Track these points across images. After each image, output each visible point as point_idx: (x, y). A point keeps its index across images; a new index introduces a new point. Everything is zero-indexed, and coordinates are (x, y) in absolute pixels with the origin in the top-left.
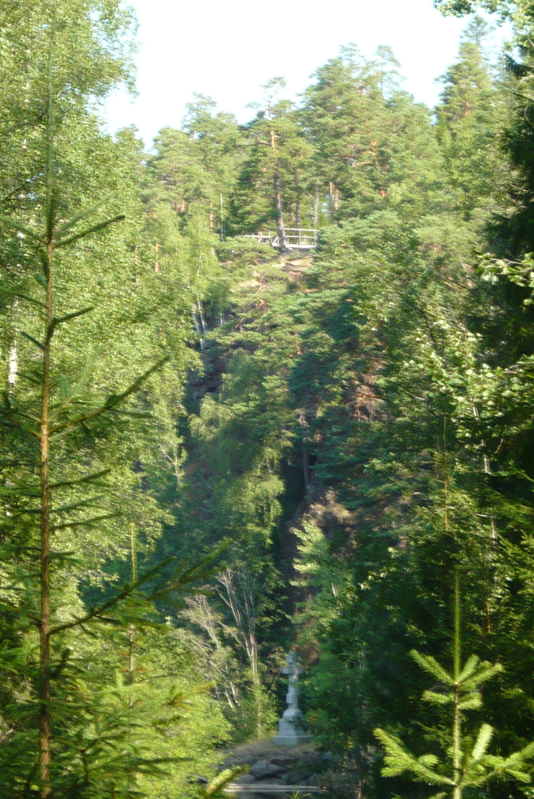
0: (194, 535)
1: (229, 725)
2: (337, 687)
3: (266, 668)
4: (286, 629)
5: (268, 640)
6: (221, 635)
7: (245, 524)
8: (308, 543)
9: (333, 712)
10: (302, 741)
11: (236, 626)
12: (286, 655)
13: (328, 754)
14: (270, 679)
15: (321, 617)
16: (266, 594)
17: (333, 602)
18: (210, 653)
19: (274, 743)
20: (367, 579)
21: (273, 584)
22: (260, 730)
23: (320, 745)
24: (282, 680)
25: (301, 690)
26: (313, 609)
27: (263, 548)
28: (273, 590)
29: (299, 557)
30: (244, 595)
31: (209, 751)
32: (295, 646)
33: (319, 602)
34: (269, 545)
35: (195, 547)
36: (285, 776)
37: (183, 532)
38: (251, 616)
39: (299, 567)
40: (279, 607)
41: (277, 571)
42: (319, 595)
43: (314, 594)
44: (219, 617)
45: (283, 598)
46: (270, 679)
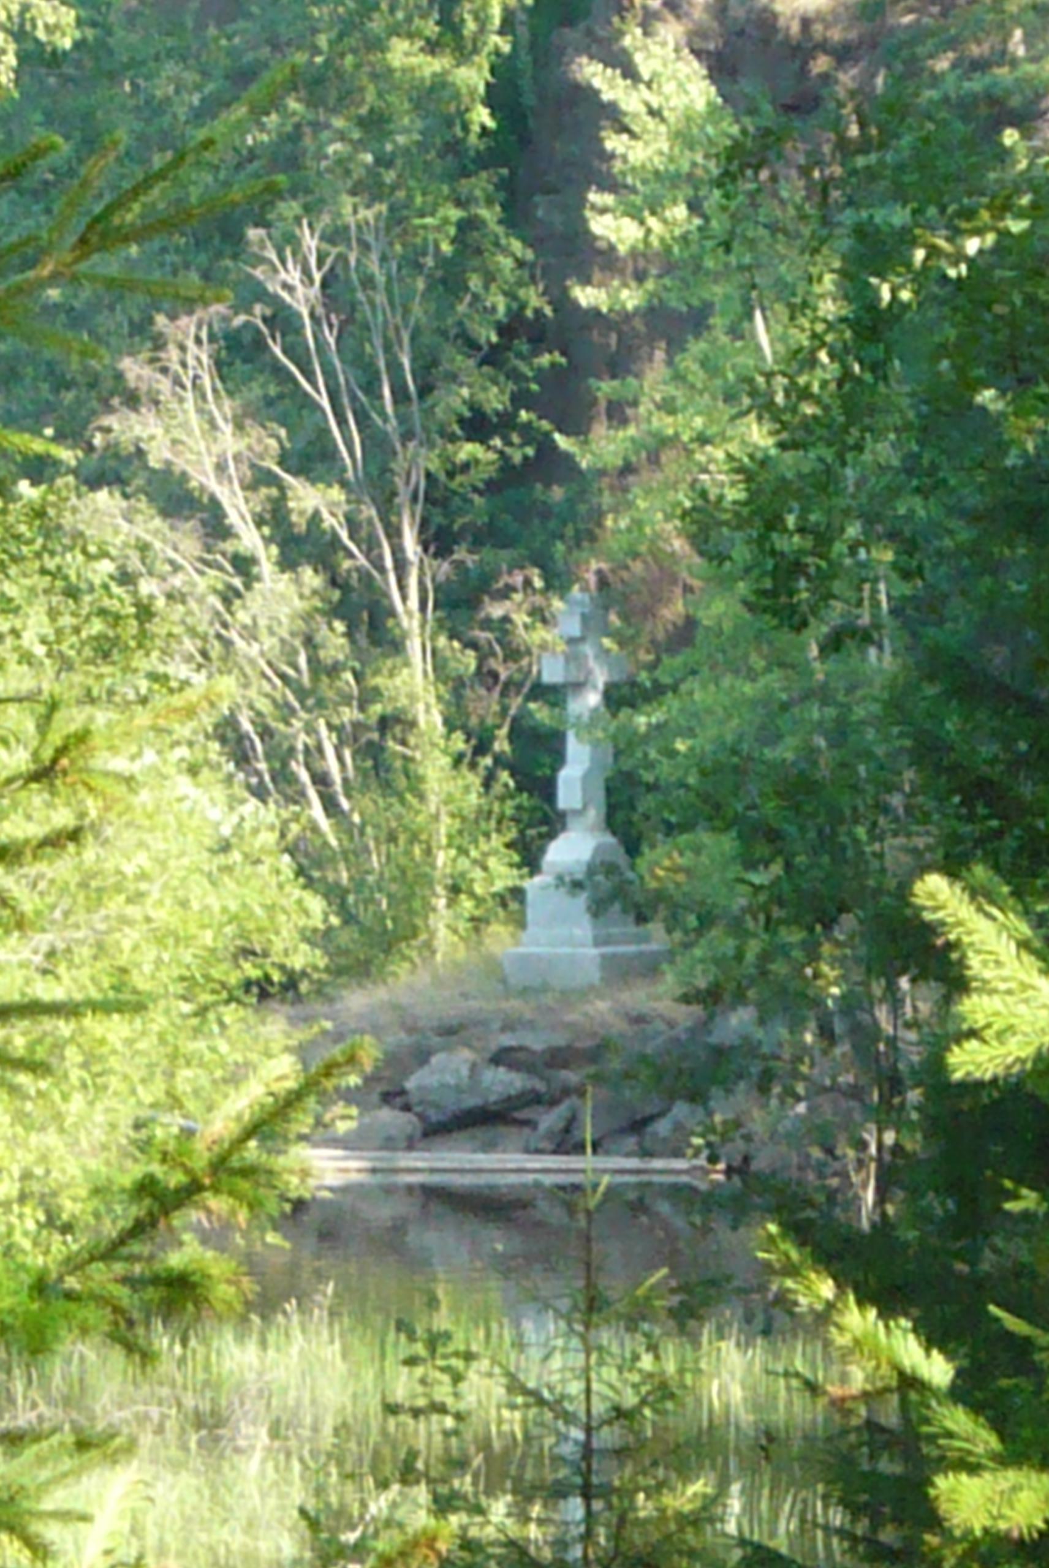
0: (163, 89)
1: (316, 904)
4: (557, 493)
6: (275, 518)
7: (378, 45)
8: (651, 123)
9: (760, 839)
10: (619, 972)
11: (344, 484)
12: (557, 604)
14: (485, 705)
15: (703, 440)
16: (471, 345)
18: (229, 596)
20: (908, 265)
22: (444, 924)
24: (540, 713)
25: (617, 754)
26: (668, 407)
27: (454, 147)
29: (611, 185)
30: (375, 350)
31: (230, 1014)
33: (697, 375)
36: (550, 1120)
37: (113, 77)
38: (407, 436)
41: (516, 246)
42: (697, 347)
43: (675, 346)
44: (268, 443)
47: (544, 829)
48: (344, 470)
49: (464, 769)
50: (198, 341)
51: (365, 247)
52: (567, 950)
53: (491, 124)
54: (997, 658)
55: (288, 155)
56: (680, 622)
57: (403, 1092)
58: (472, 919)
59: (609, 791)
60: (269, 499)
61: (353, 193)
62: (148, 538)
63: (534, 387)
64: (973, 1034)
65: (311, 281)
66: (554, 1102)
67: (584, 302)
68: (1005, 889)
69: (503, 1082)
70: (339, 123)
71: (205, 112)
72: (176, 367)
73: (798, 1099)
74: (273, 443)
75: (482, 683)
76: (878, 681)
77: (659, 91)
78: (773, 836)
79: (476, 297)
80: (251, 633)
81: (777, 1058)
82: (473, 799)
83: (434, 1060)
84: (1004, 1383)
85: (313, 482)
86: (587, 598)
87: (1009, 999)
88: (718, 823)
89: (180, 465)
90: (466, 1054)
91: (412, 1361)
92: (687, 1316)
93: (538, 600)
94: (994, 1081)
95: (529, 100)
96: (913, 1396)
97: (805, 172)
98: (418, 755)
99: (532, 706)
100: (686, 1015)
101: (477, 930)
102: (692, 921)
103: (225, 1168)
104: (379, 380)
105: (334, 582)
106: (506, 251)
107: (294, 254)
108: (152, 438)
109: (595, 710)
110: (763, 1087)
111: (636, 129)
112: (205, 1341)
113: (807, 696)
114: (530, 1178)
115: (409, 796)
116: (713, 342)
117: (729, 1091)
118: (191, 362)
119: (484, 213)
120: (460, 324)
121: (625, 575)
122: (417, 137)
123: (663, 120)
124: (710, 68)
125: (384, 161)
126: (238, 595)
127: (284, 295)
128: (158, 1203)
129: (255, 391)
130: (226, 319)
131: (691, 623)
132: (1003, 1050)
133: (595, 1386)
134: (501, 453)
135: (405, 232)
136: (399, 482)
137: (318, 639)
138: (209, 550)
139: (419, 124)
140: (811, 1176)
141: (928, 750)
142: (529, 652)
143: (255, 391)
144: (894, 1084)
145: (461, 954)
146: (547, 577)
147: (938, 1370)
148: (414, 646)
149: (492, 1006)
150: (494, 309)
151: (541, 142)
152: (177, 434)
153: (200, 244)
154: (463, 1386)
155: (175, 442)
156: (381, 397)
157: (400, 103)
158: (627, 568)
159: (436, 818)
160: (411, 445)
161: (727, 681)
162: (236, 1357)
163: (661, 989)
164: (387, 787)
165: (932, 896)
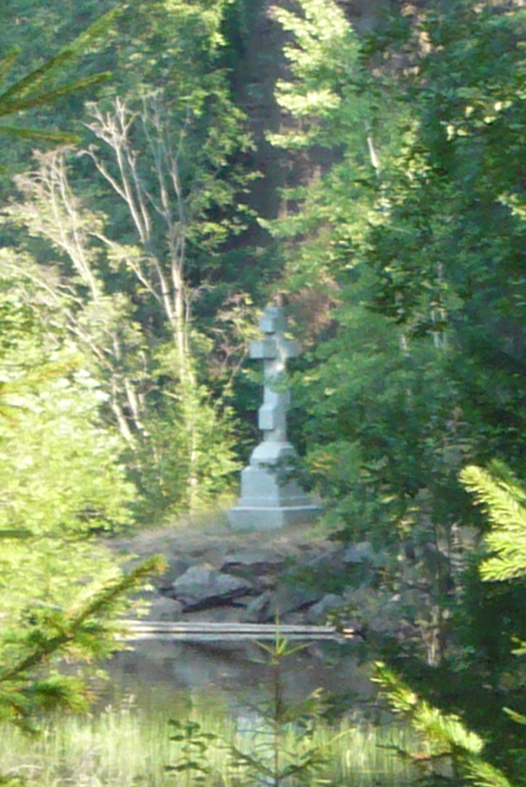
2: (380, 389)
3: (209, 344)
4: (260, 251)
5: (218, 276)
6: (100, 264)
8: (313, 42)
9: (373, 445)
10: (295, 520)
11: (140, 245)
12: (259, 313)
13: (361, 549)
14: (220, 371)
15: (341, 220)
16: (211, 168)
17: (371, 186)
18: (75, 308)
19: (228, 525)
21: (228, 144)
22: (195, 492)
23: (341, 526)
25: (293, 398)
26: (321, 202)
27: (203, 56)
28: (228, 158)
29: (291, 78)
30: (157, 169)
32: (278, 292)
33: (338, 185)
34: (219, 48)
35: (39, 52)
36: (255, 603)
38: (175, 218)
39: (291, 101)
40: (239, 198)
41: (237, 112)
42: (338, 169)
43: (326, 168)
44: (97, 222)
45: (253, 175)
46: (220, 371)
47: (251, 440)
48: (139, 237)
49: (207, 407)
50: (58, 164)
51: (152, 112)
52: (264, 509)
53: (223, 43)
54: (508, 343)
55: (108, 60)
56: (329, 323)
57: (172, 589)
58: (211, 491)
59: (289, 419)
60: (98, 254)
61: (144, 82)
62: (29, 276)
63: (246, 191)
64: (495, 554)
65: (121, 132)
66: (257, 594)
67: (273, 143)
68: (511, 473)
69: (228, 582)
70: (137, 42)
71: (63, 36)
72: (45, 180)
73: (396, 592)
74: (99, 222)
75: (218, 357)
76: (440, 356)
77: (319, 27)
78: (383, 444)
79: (214, 141)
80: (87, 329)
81: (383, 569)
82: (211, 423)
83: (190, 571)
84: (513, 751)
85: (123, 244)
86: (275, 310)
87: (514, 534)
88: (349, 437)
89: (48, 233)
90: (208, 567)
91: (178, 738)
92: (333, 715)
93: (248, 311)
94: (506, 581)
95: (244, 30)
96: (460, 758)
97: (400, 70)
98: (180, 398)
99: (244, 371)
100: (332, 546)
101: (214, 497)
102: (336, 491)
103: (79, 630)
104: (159, 187)
105: (134, 301)
106: (231, 114)
107: (112, 116)
108: (31, 219)
109: (280, 374)
110: (376, 585)
111: (305, 47)
112: (62, 728)
113: (400, 366)
114: (243, 636)
115: (175, 421)
116: (347, 165)
117: (357, 588)
118: (53, 176)
119: (218, 93)
120: (205, 155)
121: (297, 297)
122: (179, 50)
123: (320, 42)
124: (346, 12)
125: (163, 63)
126: (80, 308)
127: (106, 139)
128: (42, 647)
129: (90, 193)
130: (73, 152)
131: (335, 324)
132: (511, 564)
133: (281, 754)
134: (228, 228)
135: (174, 104)
136: (171, 245)
137: (124, 332)
138: (63, 282)
139: (182, 43)
140: (401, 636)
141: (472, 396)
142: (243, 341)
143: (90, 193)
144: (449, 583)
145: (205, 509)
146: (253, 298)
147: (474, 743)
148: (179, 336)
149: (220, 539)
150: (223, 148)
151: (250, 54)
152: (46, 217)
153: (59, 109)
154: (207, 753)
155: (45, 221)
156: (159, 196)
157: (172, 32)
158: (298, 293)
159: (190, 434)
160: (177, 224)
161: (355, 356)
162: (78, 737)
163: (317, 530)
164: (163, 415)
165: (470, 478)
